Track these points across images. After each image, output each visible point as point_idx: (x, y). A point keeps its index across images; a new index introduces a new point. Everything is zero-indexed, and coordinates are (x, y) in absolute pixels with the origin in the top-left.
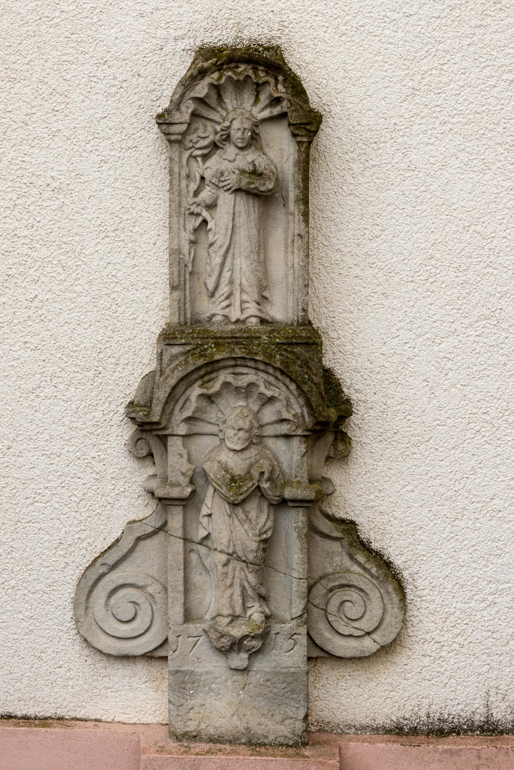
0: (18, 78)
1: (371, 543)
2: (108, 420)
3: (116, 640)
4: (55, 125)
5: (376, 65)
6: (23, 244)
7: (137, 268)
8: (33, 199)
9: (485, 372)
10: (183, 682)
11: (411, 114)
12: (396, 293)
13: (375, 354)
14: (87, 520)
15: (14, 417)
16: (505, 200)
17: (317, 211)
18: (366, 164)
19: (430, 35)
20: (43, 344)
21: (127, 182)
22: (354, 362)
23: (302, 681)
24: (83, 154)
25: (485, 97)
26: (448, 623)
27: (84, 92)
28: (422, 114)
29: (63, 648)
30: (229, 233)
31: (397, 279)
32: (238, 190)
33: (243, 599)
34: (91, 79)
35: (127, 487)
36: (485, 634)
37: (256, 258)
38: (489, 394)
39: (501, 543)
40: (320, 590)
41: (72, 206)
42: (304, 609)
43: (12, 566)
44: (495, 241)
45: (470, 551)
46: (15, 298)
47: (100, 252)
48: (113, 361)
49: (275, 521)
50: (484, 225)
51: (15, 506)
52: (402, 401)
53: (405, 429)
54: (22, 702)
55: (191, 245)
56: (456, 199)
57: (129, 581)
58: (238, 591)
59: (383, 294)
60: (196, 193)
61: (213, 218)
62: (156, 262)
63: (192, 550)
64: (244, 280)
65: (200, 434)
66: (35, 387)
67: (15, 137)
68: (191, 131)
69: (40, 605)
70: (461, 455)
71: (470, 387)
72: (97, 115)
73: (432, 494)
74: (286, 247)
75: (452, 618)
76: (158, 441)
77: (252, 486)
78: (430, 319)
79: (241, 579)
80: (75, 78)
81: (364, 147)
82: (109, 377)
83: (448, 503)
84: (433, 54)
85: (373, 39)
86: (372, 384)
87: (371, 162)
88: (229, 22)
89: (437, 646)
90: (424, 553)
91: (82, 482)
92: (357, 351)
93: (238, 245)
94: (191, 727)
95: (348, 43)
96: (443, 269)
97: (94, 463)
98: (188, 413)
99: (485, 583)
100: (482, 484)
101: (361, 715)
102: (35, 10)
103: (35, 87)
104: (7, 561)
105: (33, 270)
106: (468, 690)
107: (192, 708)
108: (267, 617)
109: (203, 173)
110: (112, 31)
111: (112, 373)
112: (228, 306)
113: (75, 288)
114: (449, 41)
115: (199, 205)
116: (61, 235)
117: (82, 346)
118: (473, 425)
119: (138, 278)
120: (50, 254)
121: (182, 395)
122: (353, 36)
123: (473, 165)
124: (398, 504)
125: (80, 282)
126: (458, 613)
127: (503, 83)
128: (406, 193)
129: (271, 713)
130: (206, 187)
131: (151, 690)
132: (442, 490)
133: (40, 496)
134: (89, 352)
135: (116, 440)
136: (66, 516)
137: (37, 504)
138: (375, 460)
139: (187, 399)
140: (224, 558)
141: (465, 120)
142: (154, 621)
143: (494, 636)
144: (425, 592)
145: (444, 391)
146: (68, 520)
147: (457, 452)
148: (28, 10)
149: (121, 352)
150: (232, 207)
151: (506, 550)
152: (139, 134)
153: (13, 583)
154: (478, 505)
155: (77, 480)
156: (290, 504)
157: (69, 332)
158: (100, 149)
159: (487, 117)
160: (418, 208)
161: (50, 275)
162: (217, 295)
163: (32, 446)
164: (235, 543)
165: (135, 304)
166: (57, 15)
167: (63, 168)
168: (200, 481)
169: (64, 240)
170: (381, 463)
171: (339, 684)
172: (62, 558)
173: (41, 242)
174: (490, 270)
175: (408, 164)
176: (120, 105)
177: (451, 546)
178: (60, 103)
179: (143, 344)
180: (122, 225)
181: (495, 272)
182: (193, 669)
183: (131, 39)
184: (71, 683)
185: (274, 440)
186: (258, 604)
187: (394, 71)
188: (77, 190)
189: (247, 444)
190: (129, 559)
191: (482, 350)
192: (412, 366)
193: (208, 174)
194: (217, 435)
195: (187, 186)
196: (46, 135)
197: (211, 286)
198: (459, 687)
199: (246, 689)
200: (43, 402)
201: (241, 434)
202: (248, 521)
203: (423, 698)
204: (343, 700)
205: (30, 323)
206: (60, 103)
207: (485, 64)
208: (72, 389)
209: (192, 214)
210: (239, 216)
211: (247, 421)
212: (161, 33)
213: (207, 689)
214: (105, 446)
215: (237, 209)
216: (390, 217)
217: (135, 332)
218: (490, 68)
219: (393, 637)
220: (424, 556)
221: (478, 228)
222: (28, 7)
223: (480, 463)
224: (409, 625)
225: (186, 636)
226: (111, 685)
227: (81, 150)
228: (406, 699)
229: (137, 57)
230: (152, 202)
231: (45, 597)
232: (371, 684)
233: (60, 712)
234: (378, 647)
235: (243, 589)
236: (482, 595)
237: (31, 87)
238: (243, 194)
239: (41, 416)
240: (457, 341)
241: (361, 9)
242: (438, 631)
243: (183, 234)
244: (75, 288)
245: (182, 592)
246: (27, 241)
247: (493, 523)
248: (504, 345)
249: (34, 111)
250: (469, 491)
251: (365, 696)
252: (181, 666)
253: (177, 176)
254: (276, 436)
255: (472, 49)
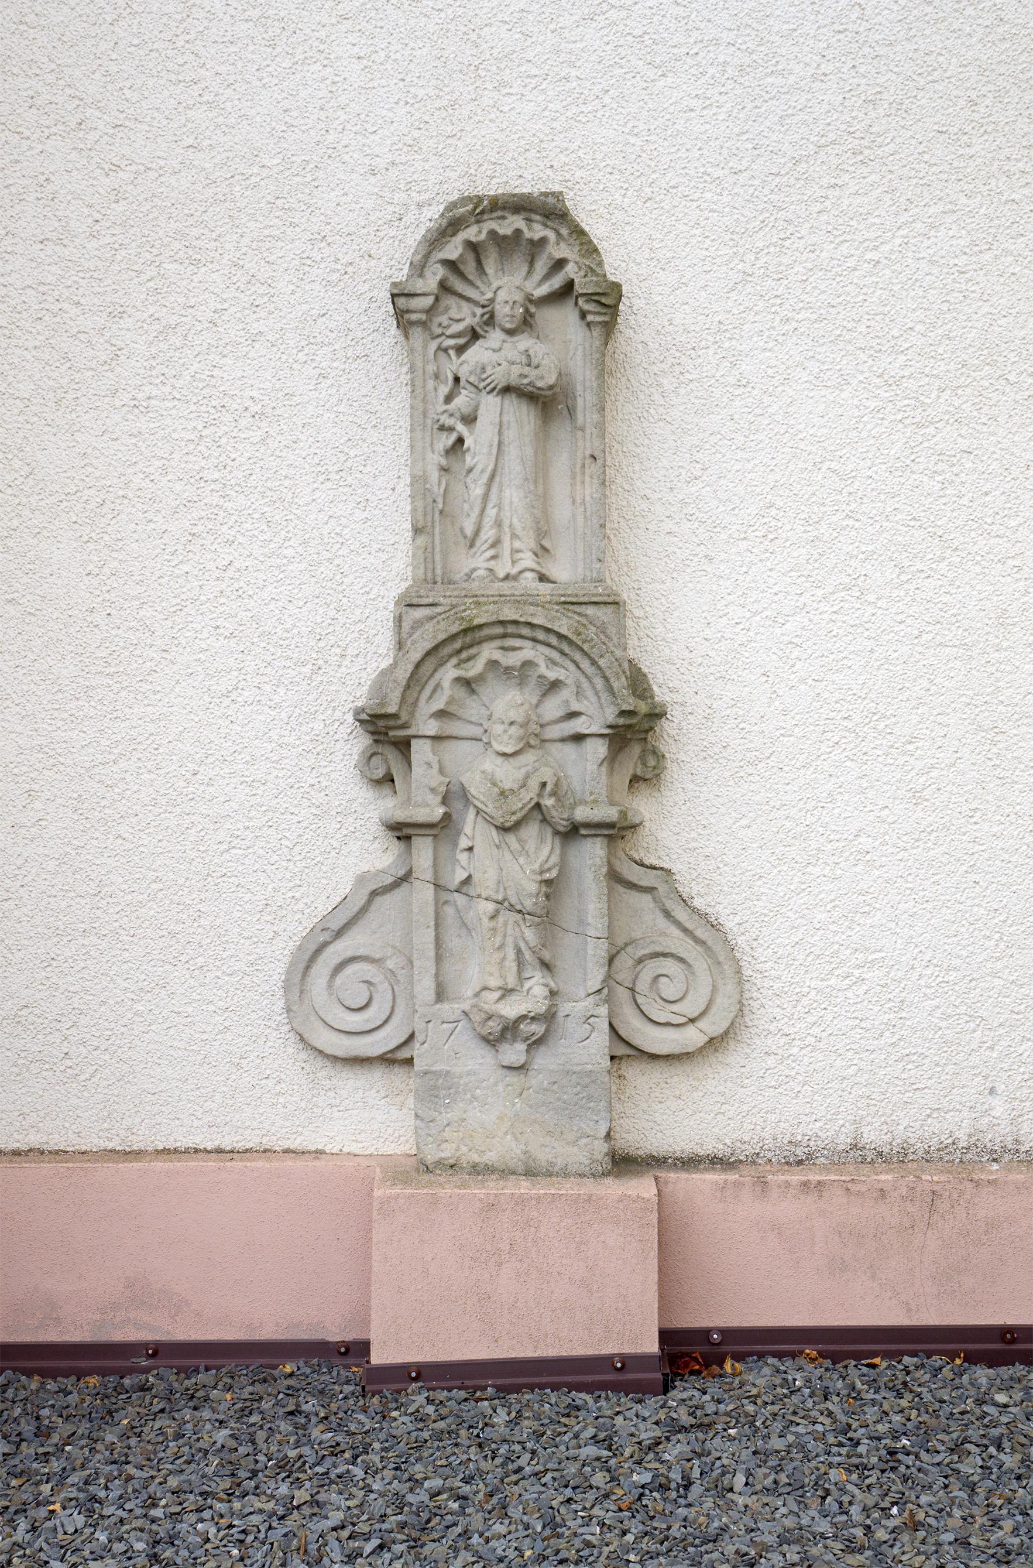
0: (203, 260)
1: (693, 898)
2: (332, 733)
3: (342, 1036)
4: (256, 325)
5: (694, 241)
6: (212, 490)
7: (369, 523)
8: (225, 428)
9: (845, 662)
10: (435, 1087)
11: (742, 308)
12: (723, 556)
13: (696, 640)
14: (303, 872)
15: (201, 730)
16: (869, 427)
17: (614, 444)
18: (681, 378)
19: (766, 199)
20: (241, 628)
21: (354, 404)
22: (667, 651)
23: (603, 1083)
24: (294, 366)
25: (842, 284)
26: (799, 1008)
27: (295, 280)
28: (756, 308)
29: (271, 1050)
30: (494, 451)
31: (724, 536)
32: (507, 390)
33: (519, 966)
34: (304, 261)
35: (358, 826)
36: (851, 1023)
37: (532, 488)
38: (851, 692)
39: (871, 896)
40: (625, 961)
41: (279, 438)
42: (604, 981)
43: (200, 937)
44: (857, 483)
45: (828, 908)
46: (202, 567)
47: (319, 501)
48: (338, 651)
49: (563, 856)
50: (842, 460)
51: (204, 855)
52: (733, 703)
53: (738, 741)
54: (214, 1129)
55: (443, 473)
56: (803, 426)
57: (361, 952)
58: (511, 955)
59: (706, 557)
60: (448, 399)
61: (471, 433)
62: (396, 514)
63: (446, 902)
64: (515, 521)
65: (456, 738)
66: (230, 688)
67: (199, 342)
68: (441, 309)
69: (239, 992)
70: (814, 776)
71: (825, 683)
72: (314, 312)
73: (776, 830)
74: (574, 478)
75: (805, 1001)
76: (396, 753)
77: (529, 802)
78: (770, 591)
79: (516, 938)
80: (282, 260)
81: (678, 354)
82: (332, 673)
83: (797, 843)
84: (771, 225)
85: (688, 204)
86: (692, 680)
87: (687, 375)
88: (493, 182)
89: (784, 1039)
90: (766, 911)
91: (296, 819)
92: (671, 635)
93: (507, 470)
94: (447, 1152)
95: (655, 212)
96: (786, 521)
97: (312, 793)
98: (439, 704)
99: (849, 951)
100: (843, 816)
101: (684, 1137)
102: (225, 164)
103: (226, 272)
104: (192, 930)
105: (226, 527)
106: (828, 1101)
107: (448, 1125)
108: (553, 994)
109: (458, 369)
110: (332, 194)
111: (336, 668)
112: (493, 557)
113: (285, 552)
114: (793, 207)
115: (451, 415)
116: (264, 478)
117: (295, 631)
118: (829, 735)
119: (372, 537)
120: (249, 504)
121: (429, 678)
122: (661, 201)
123: (826, 378)
124: (728, 845)
125: (291, 543)
126: (813, 993)
127: (866, 265)
128: (736, 417)
129: (559, 1130)
130: (462, 391)
131: (394, 1107)
132: (788, 824)
133: (238, 840)
134: (304, 640)
135: (342, 760)
136: (274, 867)
137: (233, 851)
138: (697, 785)
139: (438, 686)
140: (491, 907)
141: (814, 317)
142: (396, 1009)
143: (863, 1025)
144: (768, 966)
145: (790, 689)
146: (277, 872)
147: (809, 773)
148: (215, 165)
149: (349, 639)
150: (498, 414)
151: (877, 906)
152: (370, 338)
153: (201, 961)
154: (838, 844)
155: (290, 817)
156: (583, 832)
157: (277, 612)
158: (317, 358)
159: (844, 313)
160: (752, 437)
161: (250, 534)
162: (478, 543)
163: (227, 770)
164: (507, 885)
165: (366, 573)
166: (255, 171)
167: (268, 385)
168: (458, 805)
169: (269, 484)
170: (705, 788)
171: (652, 1095)
172: (269, 926)
173: (237, 488)
174: (851, 522)
175: (738, 377)
176: (345, 298)
177: (802, 901)
178: (262, 295)
179: (379, 628)
180: (349, 464)
181: (857, 524)
182: (448, 1068)
183: (358, 206)
184: (282, 1100)
185: (559, 745)
186: (540, 975)
187: (717, 249)
188: (286, 415)
189: (521, 745)
190: (361, 923)
191: (841, 632)
192: (746, 654)
193: (463, 374)
194: (481, 740)
195: (435, 389)
196: (243, 340)
197: (469, 531)
198: (816, 1097)
199: (524, 1096)
200: (242, 709)
201: (513, 730)
202: (524, 853)
203: (767, 1113)
204: (658, 1117)
205: (222, 600)
206: (262, 295)
207: (842, 238)
208: (282, 690)
209: (442, 428)
210: (508, 428)
211: (521, 710)
212: (400, 197)
213: (469, 1096)
214: (328, 770)
215: (505, 418)
216: (714, 450)
217: (368, 611)
218: (848, 244)
219: (725, 1025)
220: (766, 915)
221: (833, 465)
222: (216, 161)
223: (840, 787)
224: (746, 1011)
225: (439, 1021)
226: (338, 1101)
227: (291, 361)
228: (744, 1114)
229: (366, 230)
230: (390, 431)
231: (246, 980)
232: (695, 1094)
233: (267, 1142)
234: (707, 1039)
235: (519, 952)
236: (845, 969)
237: (221, 272)
238: (514, 396)
239: (239, 729)
240: (806, 620)
241: (672, 164)
242: (786, 1019)
243: (430, 455)
244: (285, 552)
245: (433, 959)
246: (217, 486)
247: (858, 869)
248: (870, 624)
249: (226, 306)
250: (825, 826)
251: (688, 1111)
252: (432, 1065)
253: (421, 372)
254: (563, 740)
255: (824, 217)
